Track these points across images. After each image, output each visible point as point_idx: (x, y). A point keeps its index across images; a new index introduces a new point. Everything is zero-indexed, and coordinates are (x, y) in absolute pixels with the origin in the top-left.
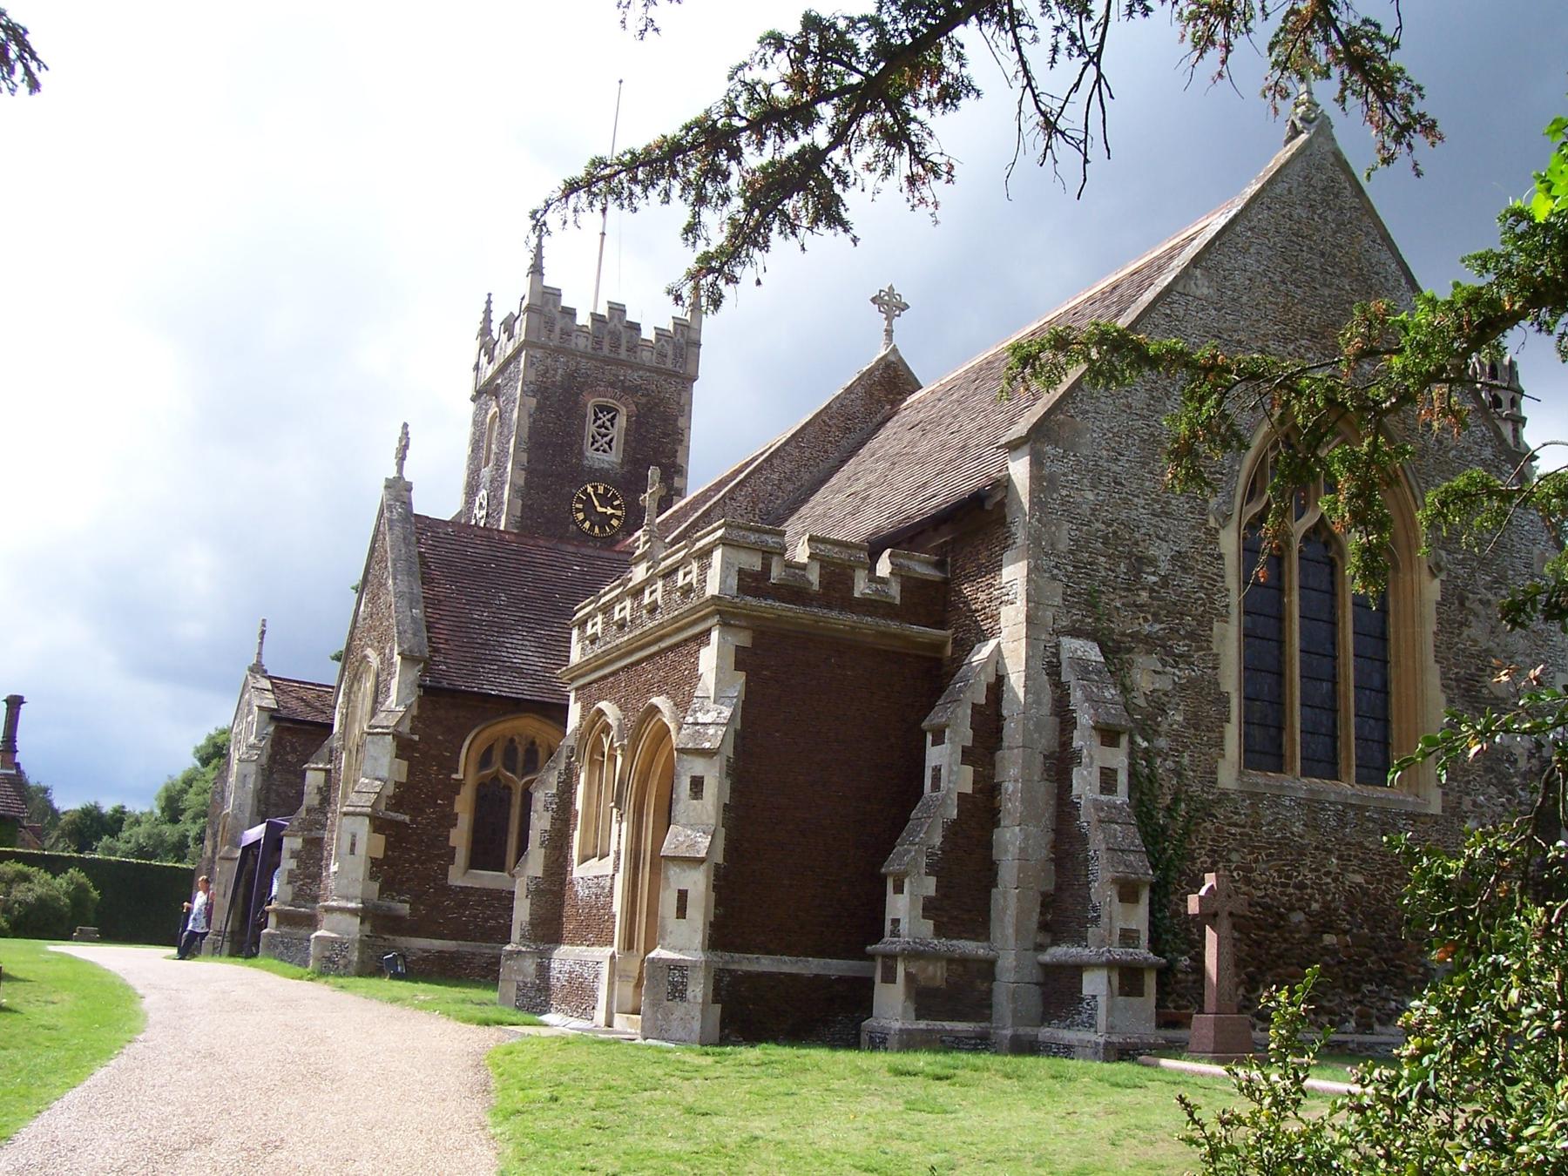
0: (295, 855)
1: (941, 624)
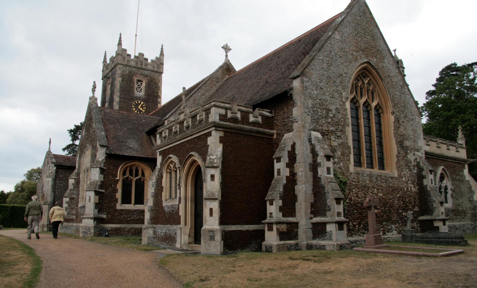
0: (67, 203)
1: (272, 129)
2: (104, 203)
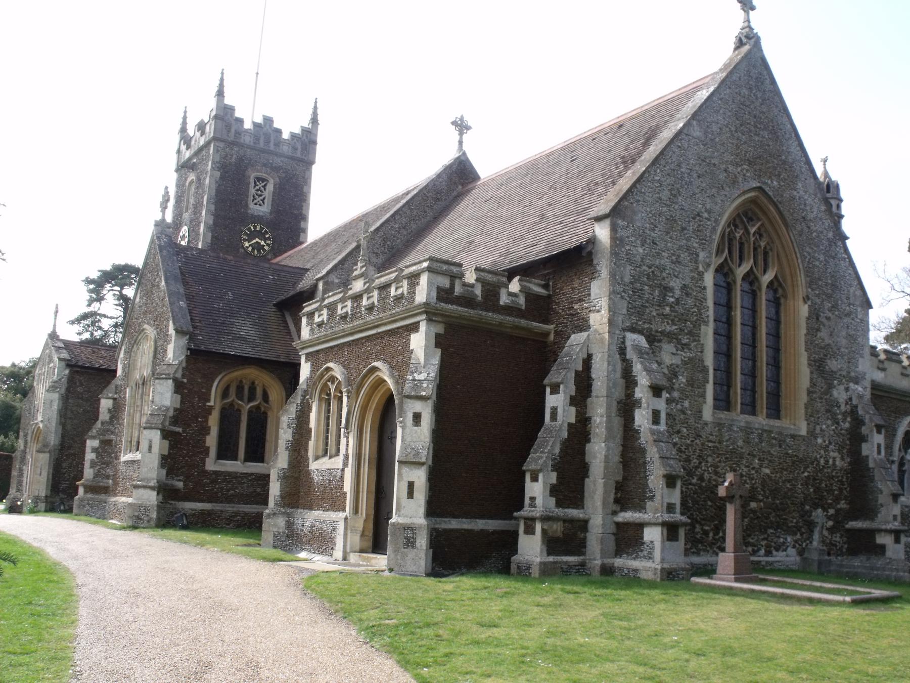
0: (94, 450)
1: (546, 321)
2: (180, 456)
